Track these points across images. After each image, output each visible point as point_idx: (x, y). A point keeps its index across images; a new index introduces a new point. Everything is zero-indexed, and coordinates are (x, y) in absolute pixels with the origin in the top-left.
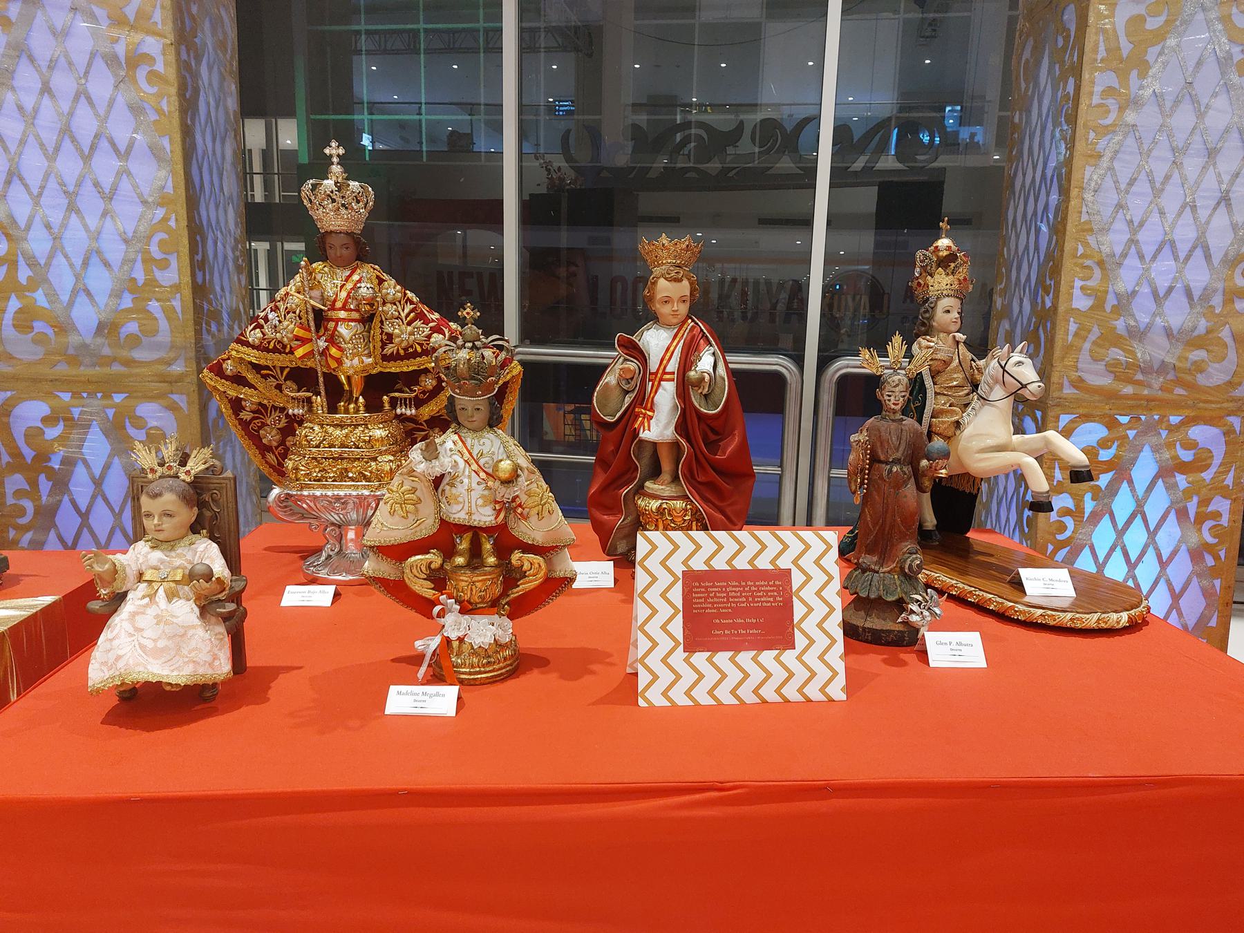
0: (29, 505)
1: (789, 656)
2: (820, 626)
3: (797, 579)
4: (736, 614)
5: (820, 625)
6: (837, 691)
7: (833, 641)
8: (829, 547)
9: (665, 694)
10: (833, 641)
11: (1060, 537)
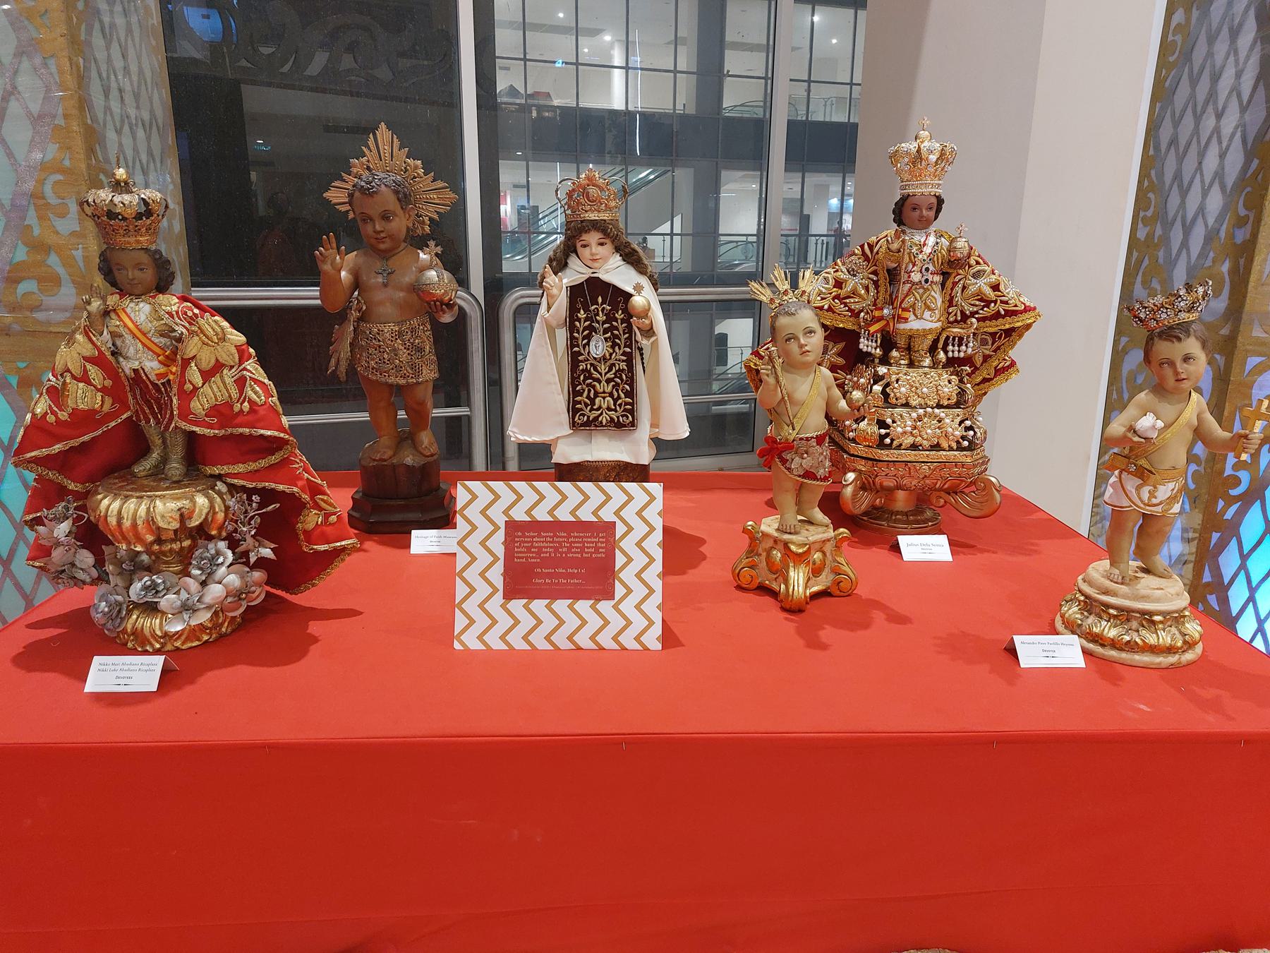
0: (1244, 476)
1: (605, 606)
3: (620, 529)
4: (558, 563)
5: (638, 576)
6: (653, 640)
11: (1234, 492)
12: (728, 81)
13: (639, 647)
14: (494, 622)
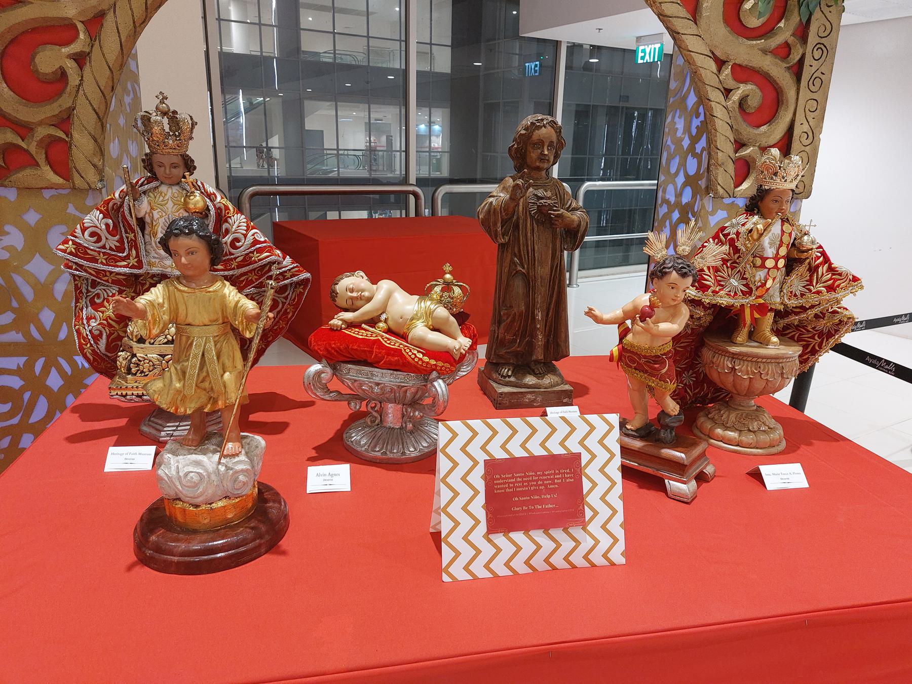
2: (601, 442)
7: (614, 483)
8: (612, 427)
9: (466, 568)
10: (614, 483)
12: (450, 44)
13: (605, 563)
14: (478, 552)
